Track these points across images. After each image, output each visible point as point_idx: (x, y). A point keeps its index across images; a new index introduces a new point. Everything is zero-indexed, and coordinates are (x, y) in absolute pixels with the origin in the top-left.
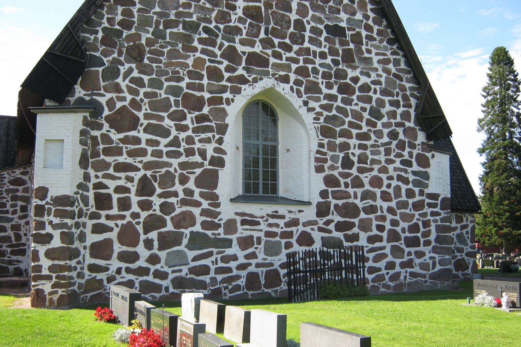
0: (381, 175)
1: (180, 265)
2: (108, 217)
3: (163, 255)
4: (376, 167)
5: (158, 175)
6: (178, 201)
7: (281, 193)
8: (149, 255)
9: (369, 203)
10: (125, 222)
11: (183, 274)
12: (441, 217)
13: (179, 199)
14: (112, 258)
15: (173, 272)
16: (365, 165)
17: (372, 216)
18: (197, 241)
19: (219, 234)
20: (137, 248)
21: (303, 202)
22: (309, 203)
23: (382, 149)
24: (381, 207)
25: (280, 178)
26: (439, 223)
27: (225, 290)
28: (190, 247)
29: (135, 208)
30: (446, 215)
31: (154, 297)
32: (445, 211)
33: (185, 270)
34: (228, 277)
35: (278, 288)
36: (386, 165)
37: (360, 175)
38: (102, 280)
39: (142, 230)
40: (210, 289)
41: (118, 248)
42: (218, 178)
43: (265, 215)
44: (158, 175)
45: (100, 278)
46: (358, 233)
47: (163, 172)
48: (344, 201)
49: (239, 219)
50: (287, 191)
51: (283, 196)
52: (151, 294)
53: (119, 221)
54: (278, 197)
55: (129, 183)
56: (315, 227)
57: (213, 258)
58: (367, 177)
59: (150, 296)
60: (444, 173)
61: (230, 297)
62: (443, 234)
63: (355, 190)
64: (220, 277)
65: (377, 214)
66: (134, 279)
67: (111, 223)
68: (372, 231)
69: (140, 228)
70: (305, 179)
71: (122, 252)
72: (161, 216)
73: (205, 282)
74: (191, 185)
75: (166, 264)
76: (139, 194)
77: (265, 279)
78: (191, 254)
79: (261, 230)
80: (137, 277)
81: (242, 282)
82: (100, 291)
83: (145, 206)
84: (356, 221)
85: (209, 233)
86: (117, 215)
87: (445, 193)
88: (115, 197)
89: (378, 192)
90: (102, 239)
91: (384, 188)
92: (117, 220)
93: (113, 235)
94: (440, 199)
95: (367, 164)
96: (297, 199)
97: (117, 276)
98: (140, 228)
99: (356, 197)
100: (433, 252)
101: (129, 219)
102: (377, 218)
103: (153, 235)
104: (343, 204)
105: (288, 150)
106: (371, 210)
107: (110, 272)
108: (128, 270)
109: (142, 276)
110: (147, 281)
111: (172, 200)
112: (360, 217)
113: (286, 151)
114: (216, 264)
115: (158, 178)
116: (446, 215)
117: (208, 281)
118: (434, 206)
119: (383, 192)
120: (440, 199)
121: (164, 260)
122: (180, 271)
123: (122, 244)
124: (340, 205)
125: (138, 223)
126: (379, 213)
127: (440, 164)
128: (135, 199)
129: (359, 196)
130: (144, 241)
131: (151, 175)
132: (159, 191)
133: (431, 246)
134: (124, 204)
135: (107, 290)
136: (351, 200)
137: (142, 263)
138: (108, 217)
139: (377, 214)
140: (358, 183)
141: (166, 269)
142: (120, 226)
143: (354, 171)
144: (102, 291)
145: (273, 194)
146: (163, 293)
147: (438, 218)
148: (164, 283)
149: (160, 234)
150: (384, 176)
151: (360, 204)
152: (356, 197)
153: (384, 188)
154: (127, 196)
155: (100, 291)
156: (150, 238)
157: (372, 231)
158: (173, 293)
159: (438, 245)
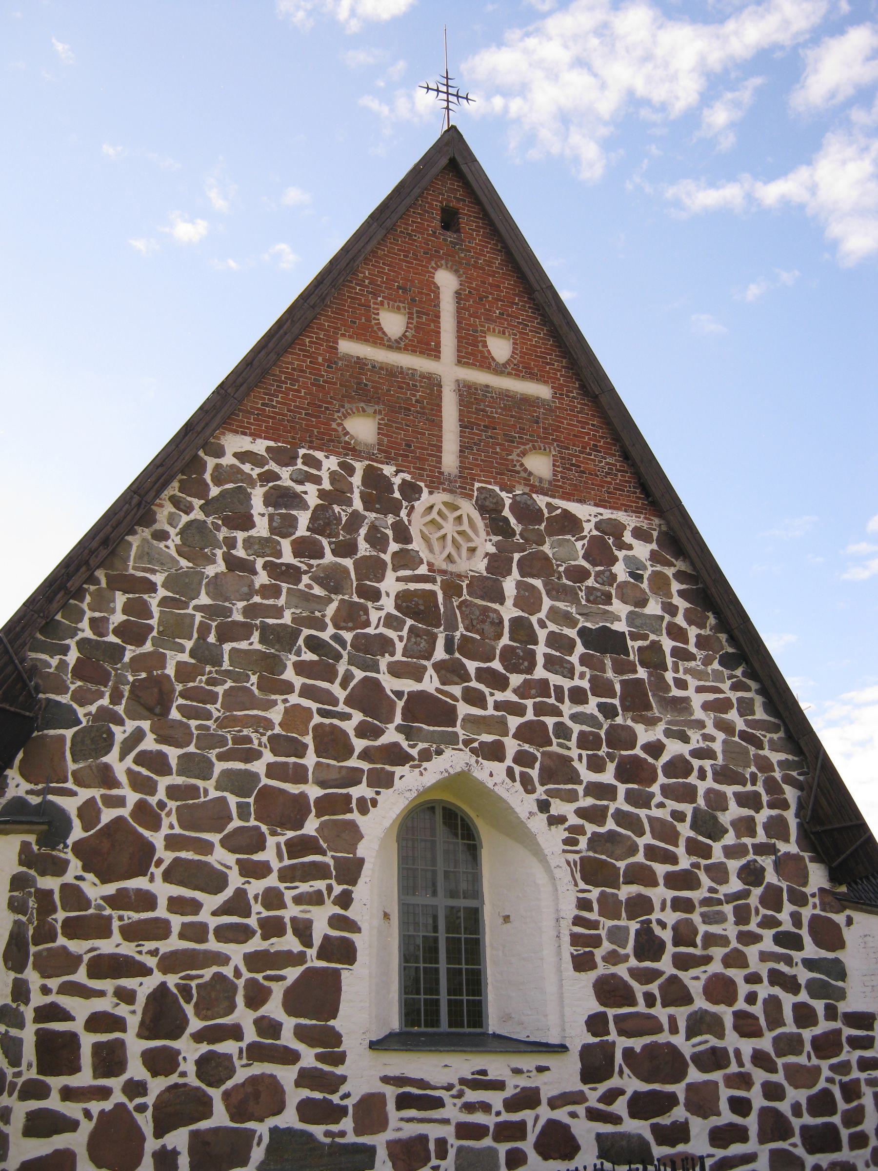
0: (731, 972)
2: (68, 1094)
4: (718, 952)
9: (706, 1042)
16: (691, 950)
17: (717, 1076)
19: (342, 1134)
22: (562, 1048)
24: (738, 1053)
29: (136, 1070)
36: (740, 947)
37: (681, 974)
43: (456, 1082)
44: (193, 984)
46: (686, 1119)
47: (207, 978)
48: (647, 1040)
56: (580, 1109)
58: (697, 978)
63: (671, 1010)
65: (728, 1071)
67: (72, 1110)
68: (718, 1114)
69: (145, 1122)
74: (274, 1008)
76: (147, 1033)
79: (446, 1121)
83: (161, 1062)
84: (679, 1089)
85: (318, 1131)
88: (88, 1041)
89: (726, 1013)
91: (740, 1004)
92: (89, 1100)
95: (695, 946)
96: (532, 1039)
98: (145, 1122)
99: (674, 1030)
101: (118, 1097)
102: (733, 1081)
104: (645, 1047)
111: (228, 1047)
115: (194, 991)
119: (739, 1015)
124: (638, 1050)
125: (141, 1108)
126: (734, 1068)
128: (135, 1046)
129: (682, 1025)
130: (155, 1155)
131: (177, 986)
132: (195, 1024)
134: (110, 1060)
136: (663, 1038)
138: (68, 1094)
139: (728, 1071)
143: (665, 965)
149: (194, 1135)
150: (737, 975)
152: (674, 1030)
153: (740, 1004)
154: (117, 1040)
156: (169, 1148)
157: (718, 1114)
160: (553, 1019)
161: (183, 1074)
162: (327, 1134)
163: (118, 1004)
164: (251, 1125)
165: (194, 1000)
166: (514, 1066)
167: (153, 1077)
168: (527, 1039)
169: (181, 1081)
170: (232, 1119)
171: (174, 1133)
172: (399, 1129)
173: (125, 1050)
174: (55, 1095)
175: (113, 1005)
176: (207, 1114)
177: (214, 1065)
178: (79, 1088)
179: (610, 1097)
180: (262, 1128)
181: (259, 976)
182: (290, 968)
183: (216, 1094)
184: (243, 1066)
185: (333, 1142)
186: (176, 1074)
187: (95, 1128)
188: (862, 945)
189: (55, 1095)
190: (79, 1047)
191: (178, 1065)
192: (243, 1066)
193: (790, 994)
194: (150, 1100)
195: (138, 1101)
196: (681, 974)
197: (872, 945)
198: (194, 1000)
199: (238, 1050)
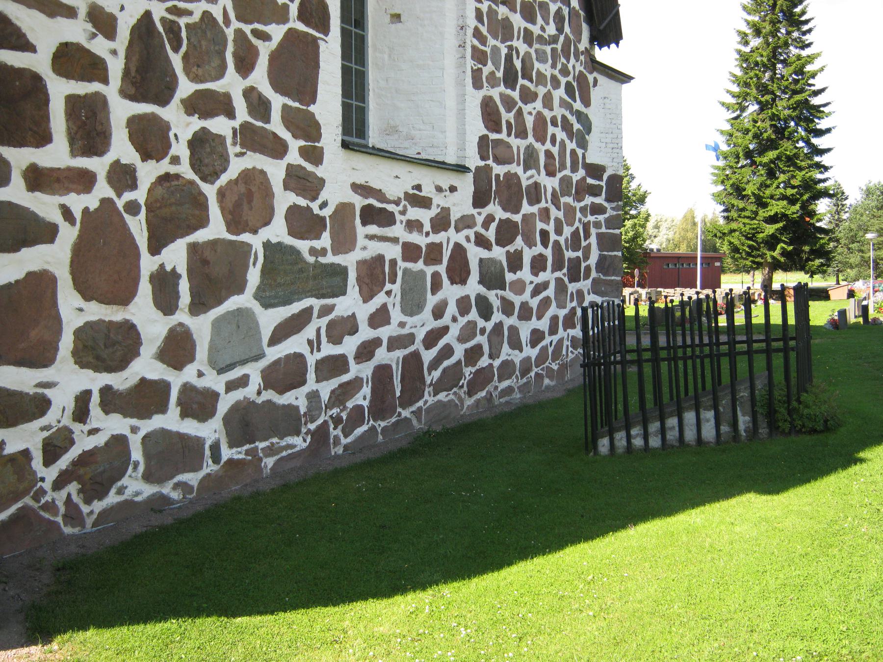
1: (243, 362)
2: (37, 179)
3: (202, 327)
5: (183, 21)
6: (235, 131)
7: (374, 138)
8: (164, 332)
10: (92, 201)
11: (249, 392)
12: (607, 215)
13: (236, 124)
14: (59, 357)
15: (231, 386)
18: (286, 276)
19: (323, 252)
20: (132, 307)
21: (443, 163)
22: (461, 169)
25: (371, 93)
26: (603, 230)
27: (335, 429)
28: (268, 297)
29: (122, 148)
30: (615, 213)
31: (184, 486)
32: (614, 205)
33: (254, 371)
34: (341, 386)
35: (420, 403)
38: (26, 454)
39: (146, 234)
40: (309, 432)
41: (74, 311)
42: (317, 66)
44: (183, 21)
45: (21, 447)
47: (196, 17)
49: (359, 202)
50: (391, 130)
51: (378, 146)
52: (175, 480)
53: (73, 195)
54: (366, 146)
55: (100, 38)
57: (309, 332)
59: (176, 486)
60: (614, 122)
61: (346, 447)
62: (610, 253)
64: (326, 389)
66: (127, 432)
67: (45, 206)
69: (138, 227)
70: (451, 102)
71: (89, 326)
72: (192, 183)
73: (297, 408)
74: (260, 78)
75: (212, 363)
76: (132, 91)
77: (401, 382)
78: (269, 319)
79: (395, 240)
80: (134, 422)
81: (365, 398)
82: (19, 505)
83: (150, 138)
85: (303, 246)
86: (69, 169)
87: (615, 164)
88: (60, 90)
90: (19, 275)
92: (67, 191)
93: (54, 257)
94: (605, 177)
96: (423, 156)
97: (77, 427)
98: (138, 227)
100: (593, 293)
101: (103, 189)
103: (175, 255)
105: (396, 18)
107: (51, 417)
108: (111, 401)
109: (149, 417)
110: (163, 433)
111: (220, 126)
113: (388, 19)
114: (319, 350)
115: (184, 34)
116: (615, 213)
117: (302, 405)
118: (594, 191)
120: (605, 177)
121: (206, 346)
122: (243, 382)
123: (87, 296)
125: (133, 208)
127: (606, 100)
128: (121, 110)
130: (153, 278)
131: (163, 20)
132: (186, 87)
133: (591, 279)
134: (89, 131)
135: (43, 492)
137: (146, 366)
138: (37, 179)
141: (215, 382)
142: (78, 216)
144: (28, 500)
145: (360, 138)
146: (209, 467)
147: (601, 218)
148: (210, 431)
149: (193, 248)
154: (97, 94)
155: (19, 505)
156: (168, 268)
158: (230, 461)
159: (602, 277)
160: (451, 137)
161: (175, 160)
162: (313, 251)
163: (94, 36)
164: (246, 237)
165: (184, 48)
166: (438, 183)
167: (143, 160)
168: (417, 156)
169: (173, 170)
170: (229, 230)
171: (172, 247)
172: (364, 248)
173: (109, 113)
174: (17, 180)
175: (87, 35)
176: (203, 222)
177: (208, 150)
178: (52, 170)
180: (256, 241)
181: (247, 29)
182: (274, 25)
183: (210, 191)
184: (237, 155)
185: (316, 261)
186: (167, 160)
187: (80, 237)
188: (602, 105)
189: (17, 180)
190: (46, 100)
191: (169, 146)
192: (237, 155)
193: (9, 64)
194: (140, 195)
195: (128, 196)
197: (609, 107)
198: (184, 48)
199: (231, 131)
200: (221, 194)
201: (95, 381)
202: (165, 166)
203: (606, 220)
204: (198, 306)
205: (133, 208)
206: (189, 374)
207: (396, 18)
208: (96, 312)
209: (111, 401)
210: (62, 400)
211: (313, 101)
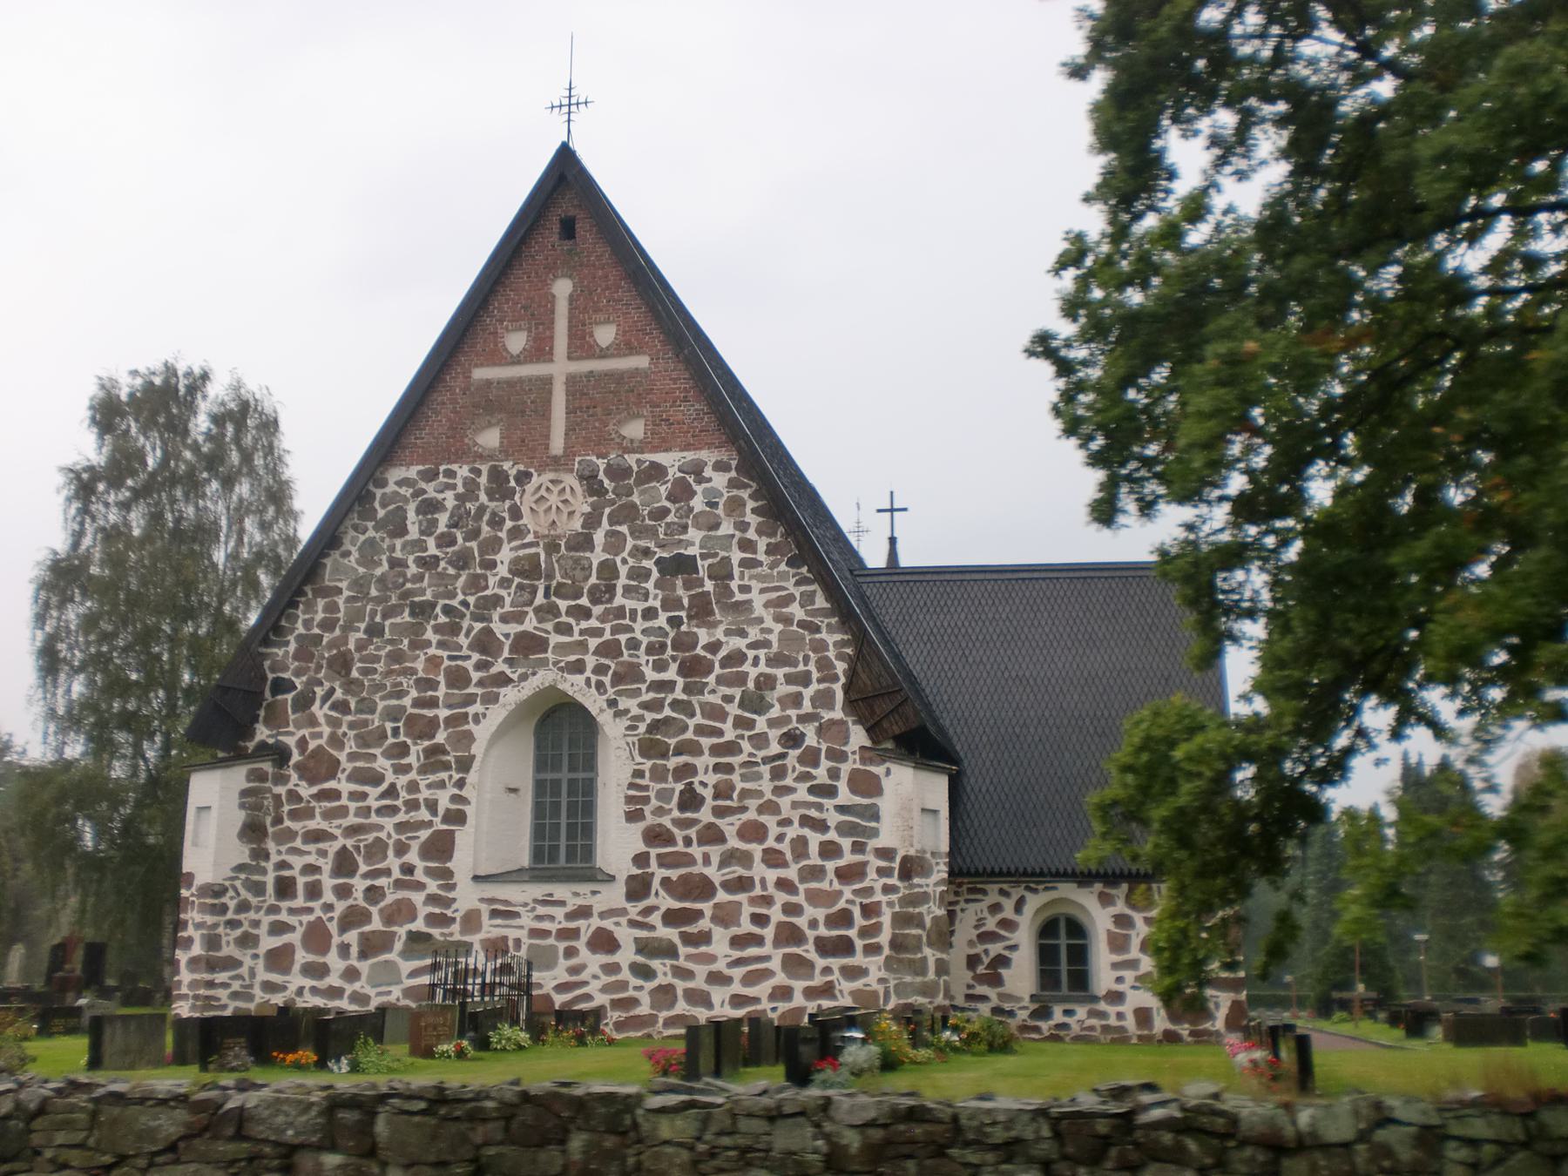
0: (764, 819)
2: (292, 911)
4: (753, 804)
10: (312, 918)
11: (392, 998)
16: (728, 803)
23: (765, 770)
24: (763, 881)
26: (897, 909)
29: (328, 896)
37: (719, 822)
41: (301, 957)
48: (683, 871)
69: (333, 927)
79: (522, 927)
89: (756, 849)
91: (770, 842)
94: (898, 860)
95: (731, 798)
98: (333, 927)
101: (318, 913)
104: (681, 877)
105: (514, 790)
106: (742, 884)
107: (287, 993)
108: (314, 991)
112: (716, 900)
129: (715, 860)
132: (363, 868)
134: (314, 891)
136: (695, 870)
137: (333, 980)
138: (292, 911)
139: (752, 894)
140: (712, 835)
143: (705, 815)
147: (894, 897)
149: (362, 934)
150: (770, 821)
151: (713, 873)
153: (770, 842)
157: (739, 925)
179: (648, 911)
196: (719, 822)
200: (381, 911)
201: (308, 983)
202: (350, 902)
203: (900, 900)
204: (363, 955)
205: (301, 923)
206: (357, 986)
207: (514, 790)
208: (311, 958)
209: (314, 991)
210: (292, 988)
211: (450, 857)
